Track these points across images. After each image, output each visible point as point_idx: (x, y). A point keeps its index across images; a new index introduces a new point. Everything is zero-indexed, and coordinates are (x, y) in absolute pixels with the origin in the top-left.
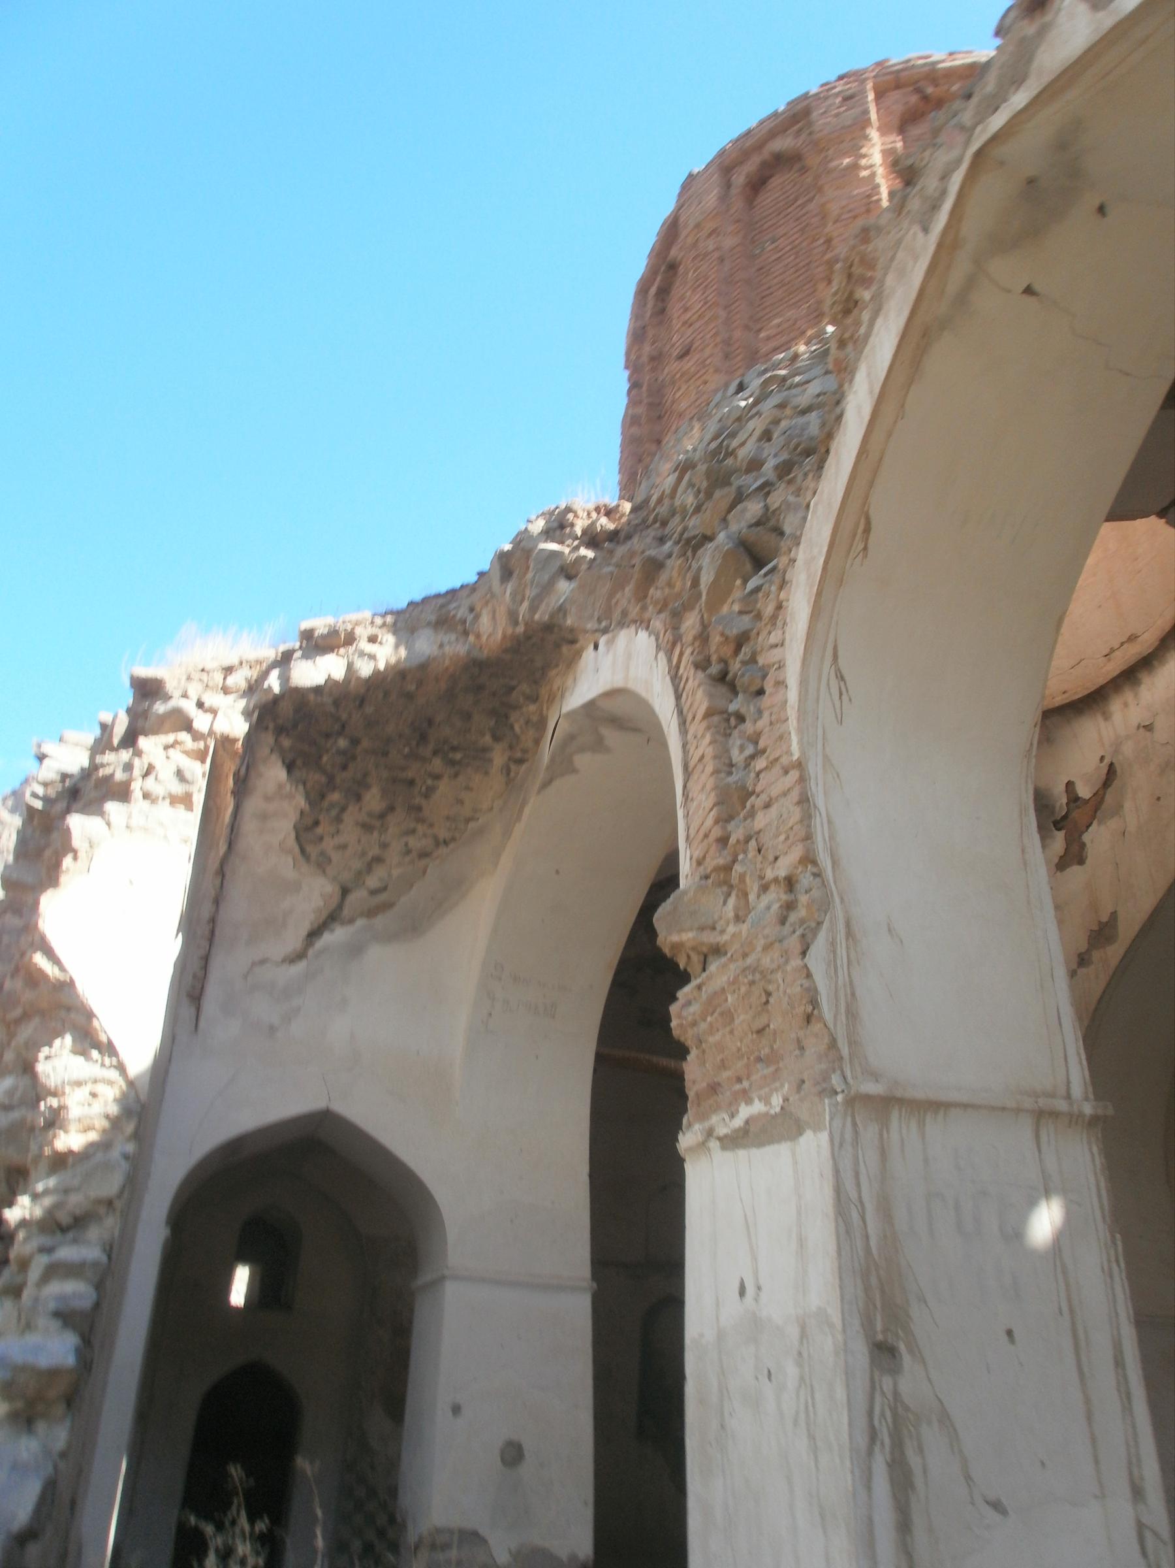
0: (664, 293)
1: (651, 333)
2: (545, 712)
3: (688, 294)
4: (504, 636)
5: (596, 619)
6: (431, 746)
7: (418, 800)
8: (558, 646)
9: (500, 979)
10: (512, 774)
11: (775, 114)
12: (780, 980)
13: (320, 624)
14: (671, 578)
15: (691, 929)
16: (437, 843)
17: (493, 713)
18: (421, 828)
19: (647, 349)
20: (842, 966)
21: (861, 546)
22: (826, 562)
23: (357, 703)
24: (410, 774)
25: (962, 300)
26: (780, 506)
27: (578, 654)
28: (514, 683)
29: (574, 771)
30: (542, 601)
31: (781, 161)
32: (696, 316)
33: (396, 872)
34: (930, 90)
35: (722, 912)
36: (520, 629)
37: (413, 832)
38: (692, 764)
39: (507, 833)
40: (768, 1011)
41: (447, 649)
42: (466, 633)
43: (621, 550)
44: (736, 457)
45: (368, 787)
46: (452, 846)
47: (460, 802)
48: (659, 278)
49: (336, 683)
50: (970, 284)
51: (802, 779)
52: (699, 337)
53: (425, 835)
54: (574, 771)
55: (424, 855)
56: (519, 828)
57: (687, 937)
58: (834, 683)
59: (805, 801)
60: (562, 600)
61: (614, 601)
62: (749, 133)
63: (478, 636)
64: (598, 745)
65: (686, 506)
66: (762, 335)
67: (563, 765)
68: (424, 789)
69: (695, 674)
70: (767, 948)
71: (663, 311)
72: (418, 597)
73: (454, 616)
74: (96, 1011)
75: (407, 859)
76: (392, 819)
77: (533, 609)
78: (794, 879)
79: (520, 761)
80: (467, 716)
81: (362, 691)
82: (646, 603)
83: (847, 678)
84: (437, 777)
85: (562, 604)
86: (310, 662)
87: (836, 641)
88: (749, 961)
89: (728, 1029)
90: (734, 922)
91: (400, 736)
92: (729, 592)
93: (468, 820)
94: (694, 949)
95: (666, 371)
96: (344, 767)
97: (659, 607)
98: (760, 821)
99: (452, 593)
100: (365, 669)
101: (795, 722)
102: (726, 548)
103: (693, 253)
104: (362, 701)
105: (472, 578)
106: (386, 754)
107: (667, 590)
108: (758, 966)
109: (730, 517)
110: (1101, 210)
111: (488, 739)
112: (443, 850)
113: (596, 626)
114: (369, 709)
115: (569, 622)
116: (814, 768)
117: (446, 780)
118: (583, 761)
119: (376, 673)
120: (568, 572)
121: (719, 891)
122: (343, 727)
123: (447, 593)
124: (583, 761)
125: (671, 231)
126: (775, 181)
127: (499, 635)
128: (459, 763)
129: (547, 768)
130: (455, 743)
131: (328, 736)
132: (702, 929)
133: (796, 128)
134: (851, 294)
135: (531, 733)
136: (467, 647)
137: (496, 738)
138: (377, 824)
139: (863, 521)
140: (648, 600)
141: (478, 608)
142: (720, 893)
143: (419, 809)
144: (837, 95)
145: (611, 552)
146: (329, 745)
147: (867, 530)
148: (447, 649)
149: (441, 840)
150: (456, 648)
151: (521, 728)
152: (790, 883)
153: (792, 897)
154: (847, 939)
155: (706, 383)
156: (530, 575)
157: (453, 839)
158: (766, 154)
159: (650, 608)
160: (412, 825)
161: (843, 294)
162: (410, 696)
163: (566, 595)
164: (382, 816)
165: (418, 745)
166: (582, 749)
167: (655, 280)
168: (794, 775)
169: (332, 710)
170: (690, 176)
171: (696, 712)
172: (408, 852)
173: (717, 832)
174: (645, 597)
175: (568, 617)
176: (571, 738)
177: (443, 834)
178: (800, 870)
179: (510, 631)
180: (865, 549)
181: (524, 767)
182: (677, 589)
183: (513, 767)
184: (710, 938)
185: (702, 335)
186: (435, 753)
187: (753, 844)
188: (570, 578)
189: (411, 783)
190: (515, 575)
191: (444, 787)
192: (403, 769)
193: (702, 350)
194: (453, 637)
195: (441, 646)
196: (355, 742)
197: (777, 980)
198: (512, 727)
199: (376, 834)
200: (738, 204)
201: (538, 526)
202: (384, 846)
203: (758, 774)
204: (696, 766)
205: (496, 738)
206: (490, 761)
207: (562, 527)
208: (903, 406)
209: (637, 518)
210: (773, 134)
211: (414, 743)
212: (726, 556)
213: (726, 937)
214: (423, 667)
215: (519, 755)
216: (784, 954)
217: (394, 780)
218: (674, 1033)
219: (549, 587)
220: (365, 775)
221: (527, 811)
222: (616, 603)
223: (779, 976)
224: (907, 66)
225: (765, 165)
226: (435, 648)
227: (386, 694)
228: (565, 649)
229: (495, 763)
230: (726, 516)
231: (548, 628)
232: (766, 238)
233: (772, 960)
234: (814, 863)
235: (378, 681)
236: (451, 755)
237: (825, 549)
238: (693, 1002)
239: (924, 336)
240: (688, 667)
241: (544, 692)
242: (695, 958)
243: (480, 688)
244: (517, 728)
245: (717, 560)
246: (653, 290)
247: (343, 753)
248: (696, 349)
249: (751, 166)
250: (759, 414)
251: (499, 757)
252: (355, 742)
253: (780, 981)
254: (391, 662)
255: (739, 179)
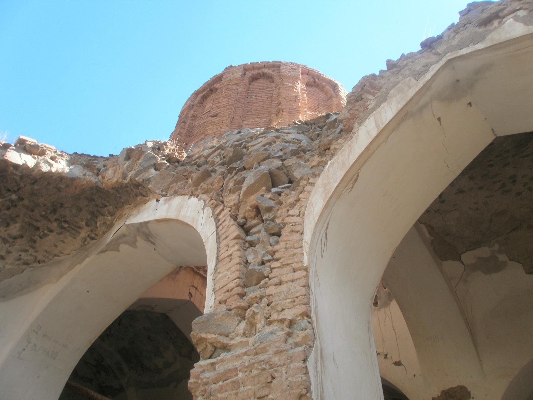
0: (205, 98)
1: (195, 108)
2: (114, 222)
3: (221, 98)
4: (117, 182)
5: (161, 190)
6: (56, 216)
7: (36, 238)
8: (136, 196)
9: (37, 333)
10: (86, 243)
11: (268, 62)
12: (283, 371)
13: (31, 140)
14: (214, 181)
15: (214, 333)
16: (35, 261)
17: (92, 213)
18: (31, 251)
19: (192, 112)
20: (319, 372)
21: (351, 186)
22: (338, 186)
23: (33, 182)
24: (39, 224)
25: (421, 110)
26: (292, 165)
27: (145, 202)
28: (107, 204)
29: (118, 251)
30: (141, 174)
31: (264, 76)
32: (222, 106)
33: (8, 267)
34: (317, 80)
35: (235, 329)
36: (126, 182)
37: (27, 251)
38: (221, 257)
39: (70, 268)
40: (269, 387)
41: (87, 177)
42: (98, 175)
43: (180, 168)
44: (248, 150)
45: (16, 222)
46: (41, 264)
47: (56, 246)
48: (205, 92)
49: (28, 167)
50: (425, 106)
51: (307, 276)
52: (223, 112)
53: (31, 255)
54: (118, 251)
55: (26, 264)
56: (78, 267)
57: (211, 337)
58: (324, 239)
59: (307, 286)
60: (150, 176)
61: (171, 186)
62: (257, 63)
63: (103, 178)
64: (133, 244)
65: (215, 161)
66: (245, 122)
67: (114, 246)
68: (42, 233)
69: (230, 219)
70: (277, 353)
71: (202, 103)
72: (80, 152)
73: (297, 82)
74: (280, 60)
75: (17, 262)
76: (19, 241)
77: (137, 175)
78: (294, 322)
79: (93, 239)
80: (80, 210)
81: (38, 177)
82: (198, 188)
83: (328, 239)
84: (51, 231)
85: (150, 178)
86: (18, 154)
87: (329, 221)
88: (262, 357)
89: (234, 392)
90: (242, 336)
91: (44, 205)
92: (257, 191)
93: (56, 255)
94: (211, 344)
95: (197, 122)
96: (8, 209)
97: (203, 192)
98: (271, 290)
99: (96, 157)
100: (45, 168)
101: (307, 250)
102: (265, 172)
103: (227, 87)
104: (35, 181)
105: (107, 155)
106: (32, 211)
107: (210, 186)
108: (269, 361)
109: (262, 163)
110: (470, 104)
111: (83, 223)
112: (36, 265)
113: (160, 193)
114: (36, 187)
115: (149, 186)
116: (312, 273)
117: (55, 233)
118: (123, 247)
119: (50, 172)
120: (156, 167)
121: (236, 318)
122: (18, 190)
123: (94, 156)
124: (123, 247)
125: (218, 79)
126: (261, 81)
127: (115, 180)
128: (65, 228)
129: (107, 245)
130: (68, 220)
131: (9, 190)
132: (220, 335)
133: (273, 69)
134: (361, 95)
135: (104, 228)
136: (96, 180)
137: (87, 225)
138: (11, 240)
139: (356, 176)
140: (199, 187)
141: (108, 167)
142: (237, 320)
143: (35, 242)
144: (290, 66)
145: (176, 167)
146: (6, 195)
147: (356, 180)
148: (87, 177)
149: (38, 260)
150: (91, 178)
151: (100, 225)
152: (291, 323)
153: (290, 331)
154: (321, 359)
155: (221, 128)
156: (140, 161)
157: (44, 261)
158: (260, 71)
159: (199, 191)
160: (27, 248)
161: (358, 94)
162: (59, 190)
163: (152, 175)
164: (15, 238)
165: (50, 213)
166: (126, 243)
167: (202, 92)
168: (300, 274)
169: (18, 178)
170: (231, 66)
171: (229, 235)
172: (20, 259)
173: (239, 290)
174: (198, 185)
175: (150, 184)
176: (124, 236)
177: (40, 257)
178: (299, 318)
179: (120, 180)
180: (352, 188)
181: (94, 241)
182: (214, 187)
183: (88, 239)
184: (224, 340)
185: (224, 112)
186: (56, 220)
187: (265, 300)
188: (156, 169)
189: (38, 229)
190: (131, 160)
191: (51, 237)
192: (37, 221)
193: (223, 117)
194: (91, 174)
195: (85, 175)
196: (21, 199)
197: (282, 371)
198: (96, 223)
199: (7, 245)
200: (246, 81)
201: (150, 144)
202: (9, 252)
203: (272, 269)
204: (224, 259)
205: (87, 225)
206: (79, 233)
207: (159, 149)
208: (388, 137)
209: (187, 160)
210: (265, 67)
211: (49, 211)
212: (264, 175)
213: (233, 342)
214: (73, 180)
215: (93, 235)
216: (289, 358)
217: (30, 224)
218: (189, 385)
219: (146, 169)
220: (17, 216)
221: (87, 260)
222: (172, 187)
223: (284, 369)
224: (313, 70)
225: (259, 74)
226: (81, 174)
227: (49, 184)
228: (139, 198)
229: (81, 235)
230: (260, 162)
231: (138, 185)
232: (253, 95)
233: (280, 360)
234: (309, 317)
235: (48, 177)
236: (63, 224)
237: (339, 181)
238: (206, 372)
239: (406, 115)
240: (227, 216)
241: (118, 214)
242: (210, 348)
243: (93, 200)
244: (98, 223)
245: (258, 175)
246: (202, 95)
247: (12, 201)
248: (220, 116)
249: (255, 72)
250: (265, 137)
251: (84, 233)
252: (21, 199)
253: (284, 372)
254: (59, 170)
255: (249, 74)
